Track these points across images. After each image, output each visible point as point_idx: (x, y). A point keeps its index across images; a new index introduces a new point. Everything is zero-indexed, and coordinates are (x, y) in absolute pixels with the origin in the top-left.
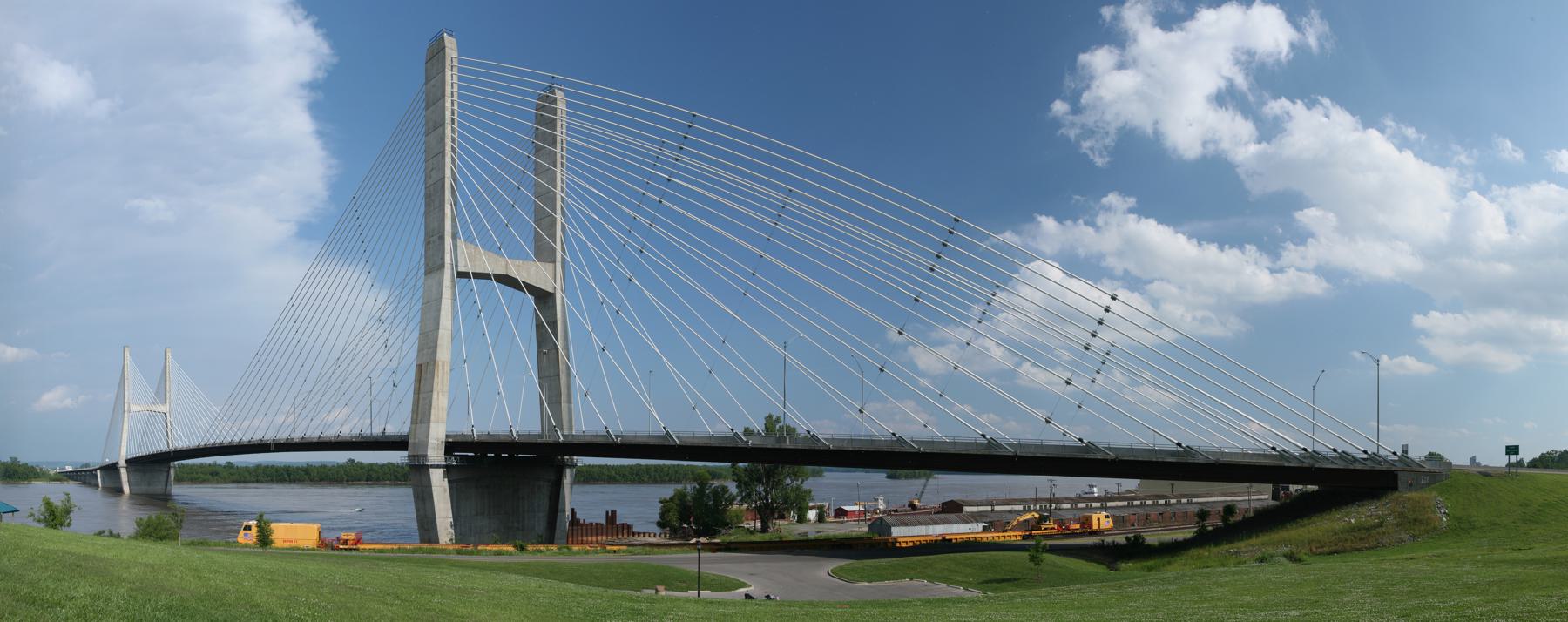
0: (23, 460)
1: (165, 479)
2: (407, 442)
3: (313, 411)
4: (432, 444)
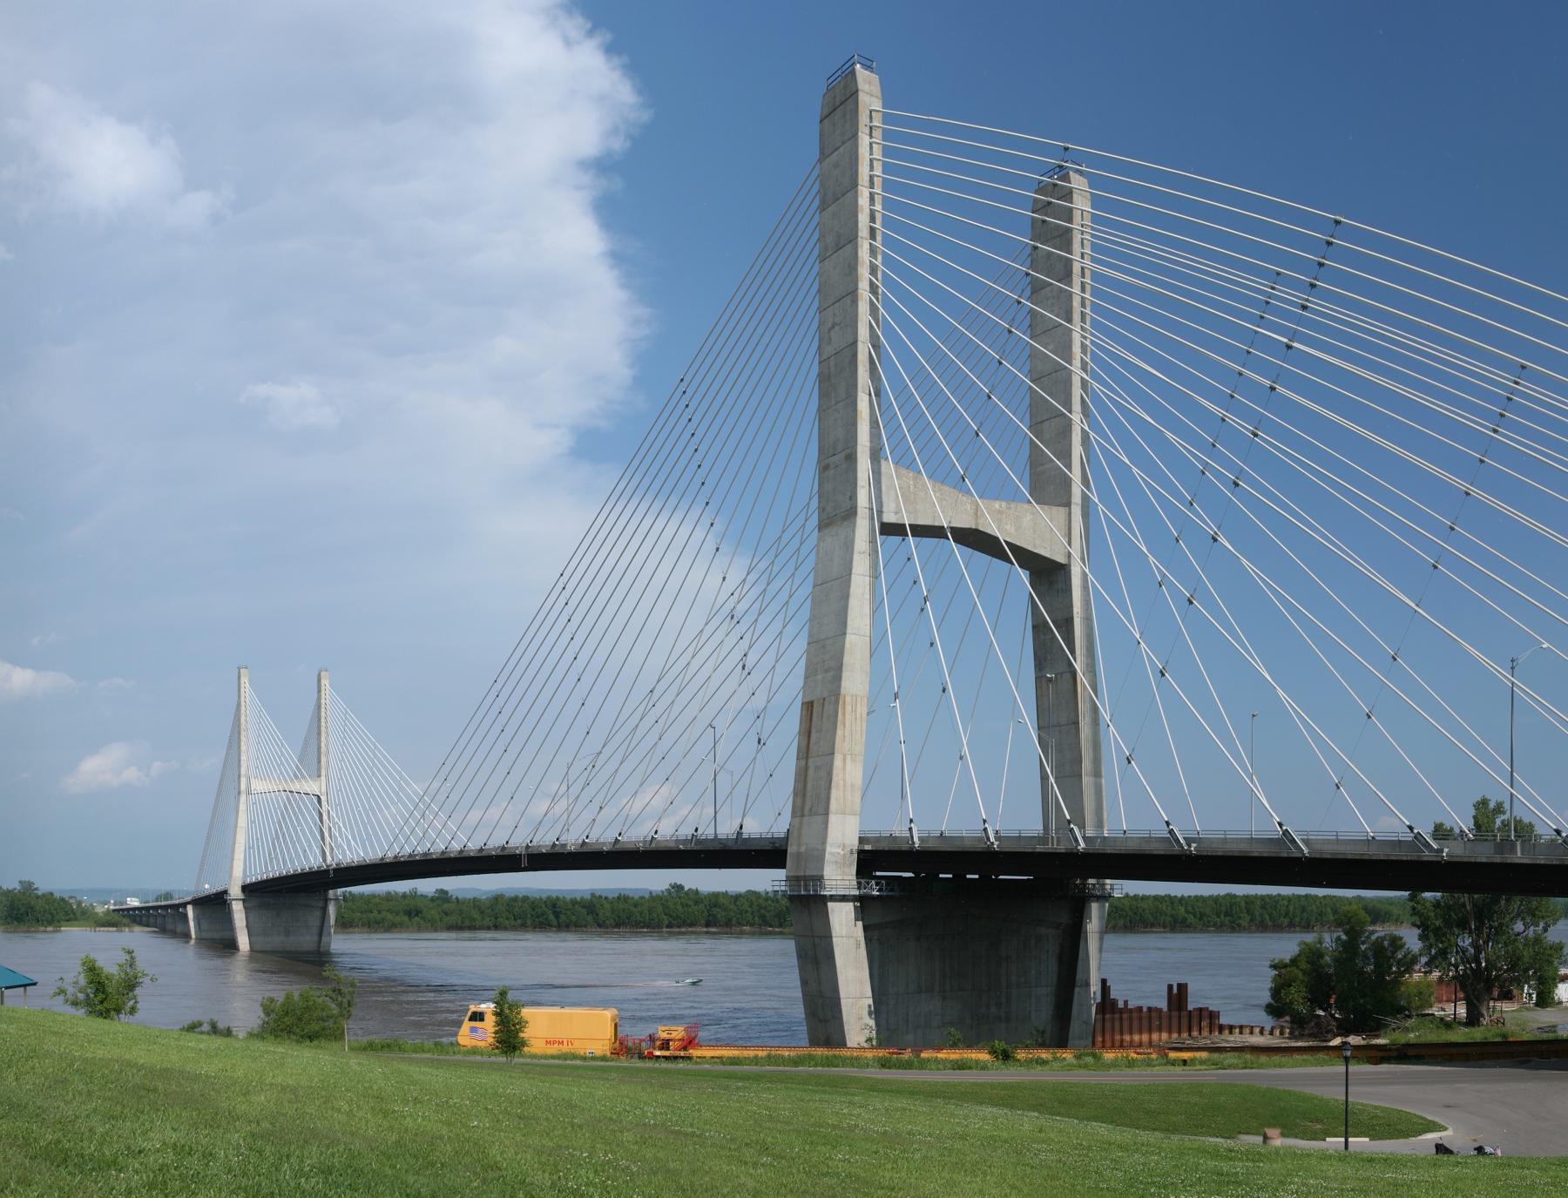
1: (317, 923)
4: (831, 853)
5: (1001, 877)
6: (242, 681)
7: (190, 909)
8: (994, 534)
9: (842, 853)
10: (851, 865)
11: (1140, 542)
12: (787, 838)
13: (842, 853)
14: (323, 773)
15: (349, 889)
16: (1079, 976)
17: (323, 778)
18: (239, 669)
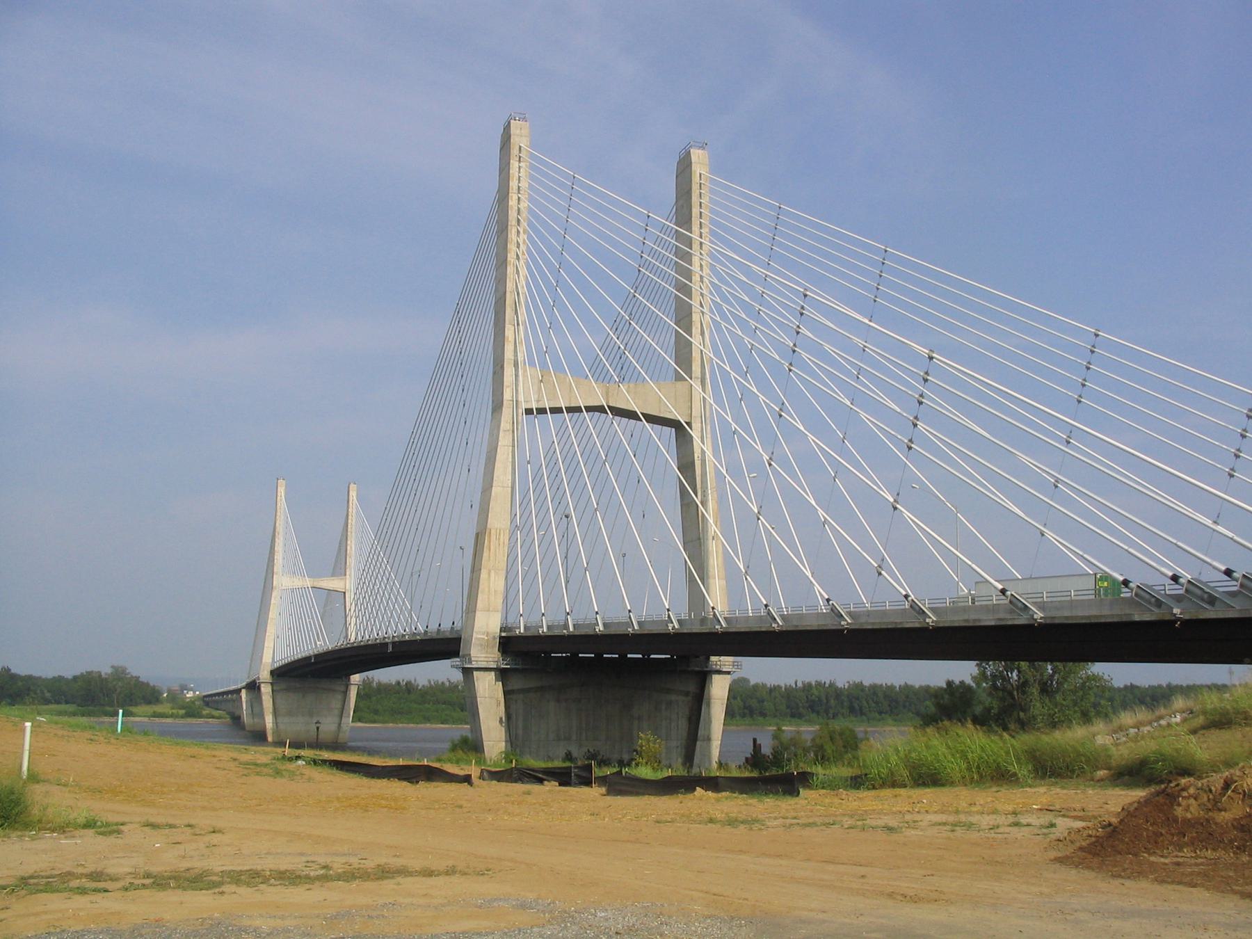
0: (1174, 683)
1: (339, 706)
2: (461, 638)
3: (414, 584)
4: (476, 638)
5: (652, 656)
6: (351, 494)
7: (244, 693)
8: (675, 418)
9: (486, 638)
10: (493, 647)
11: (796, 421)
12: (462, 629)
13: (486, 638)
14: (347, 573)
15: (370, 674)
16: (701, 733)
17: (348, 576)
18: (349, 484)
